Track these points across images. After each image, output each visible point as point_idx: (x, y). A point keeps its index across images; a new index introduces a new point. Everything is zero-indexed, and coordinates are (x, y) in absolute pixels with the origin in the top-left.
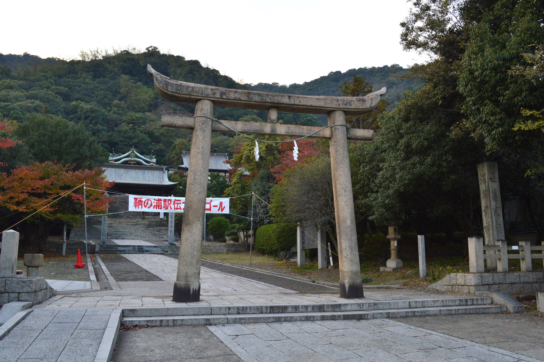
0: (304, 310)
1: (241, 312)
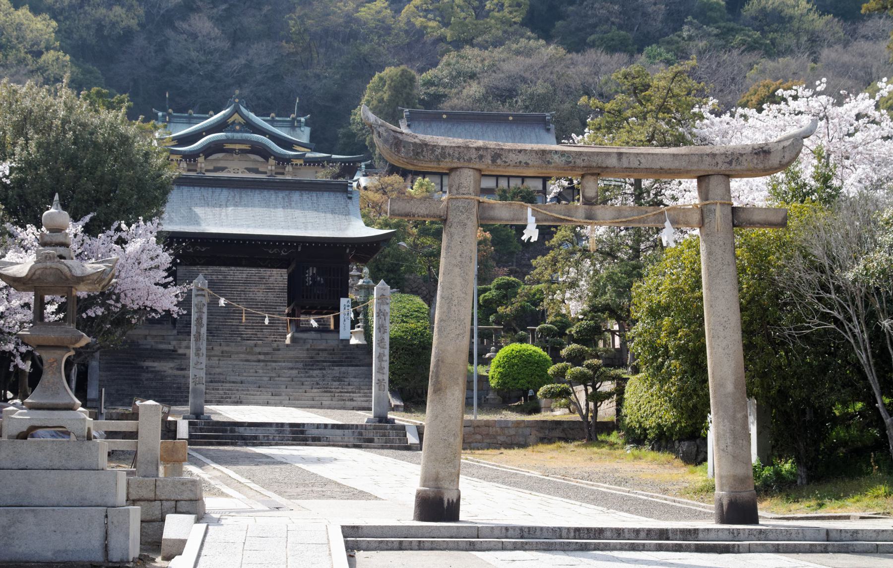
0: (633, 535)
1: (526, 535)
